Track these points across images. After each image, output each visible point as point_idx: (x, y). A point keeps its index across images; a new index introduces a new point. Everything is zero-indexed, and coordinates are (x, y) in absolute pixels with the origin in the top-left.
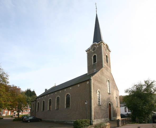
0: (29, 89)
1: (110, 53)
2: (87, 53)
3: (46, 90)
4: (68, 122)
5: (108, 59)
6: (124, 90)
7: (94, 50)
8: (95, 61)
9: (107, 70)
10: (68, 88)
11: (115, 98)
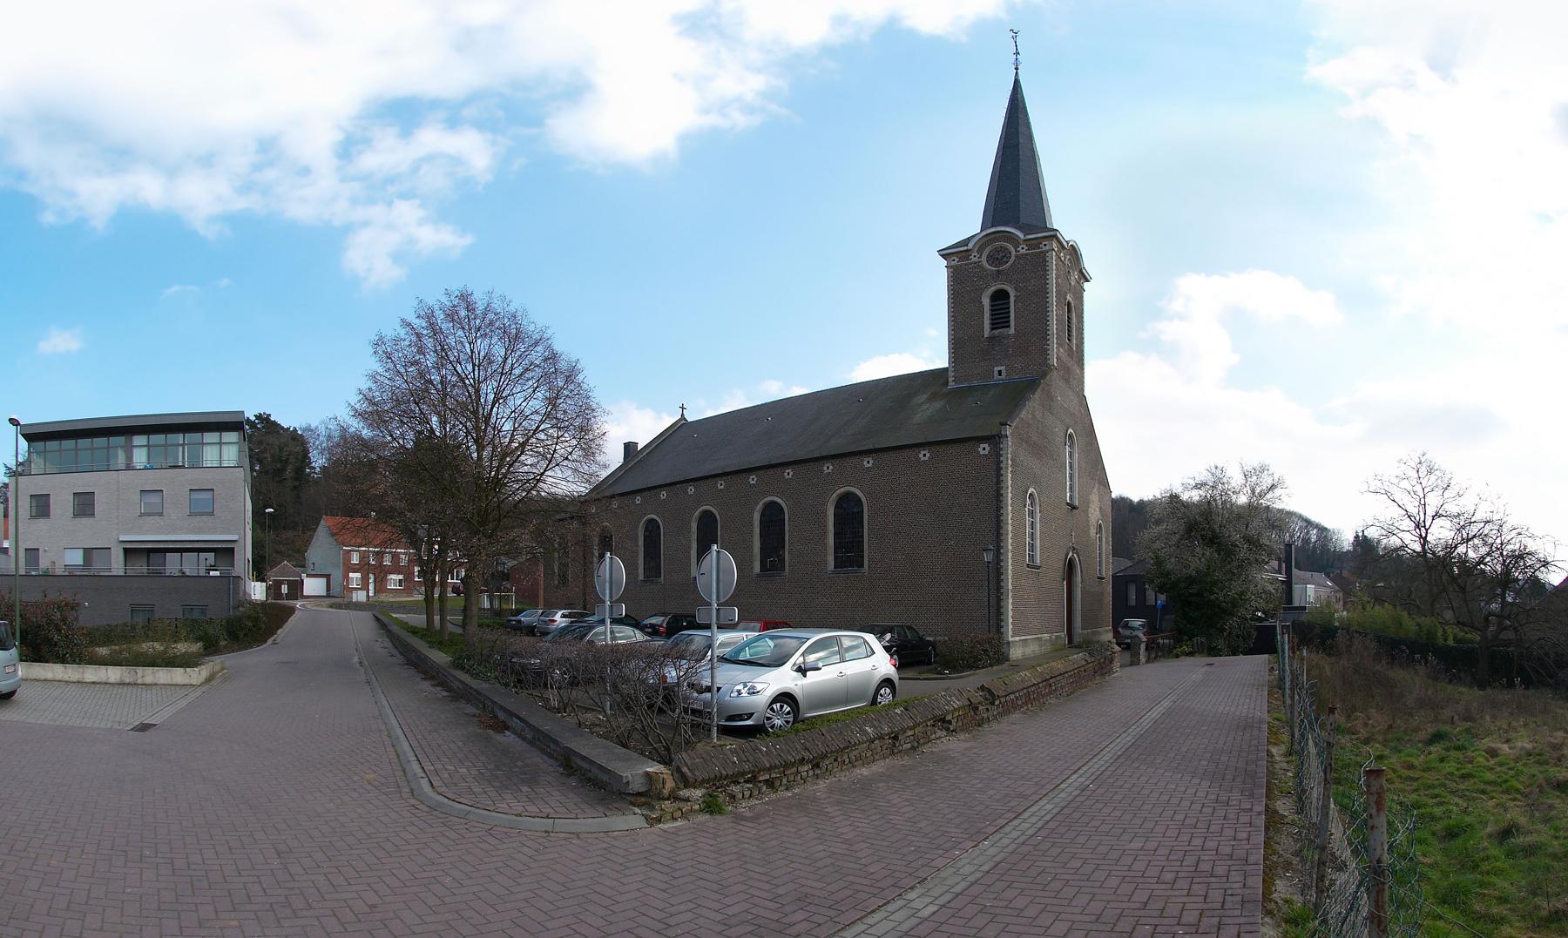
0: (365, 406)
1: (1086, 285)
2: (945, 263)
3: (629, 448)
4: (158, 646)
5: (1074, 320)
6: (456, 287)
7: (998, 257)
8: (1000, 317)
9: (1067, 381)
10: (854, 460)
11: (1093, 531)
